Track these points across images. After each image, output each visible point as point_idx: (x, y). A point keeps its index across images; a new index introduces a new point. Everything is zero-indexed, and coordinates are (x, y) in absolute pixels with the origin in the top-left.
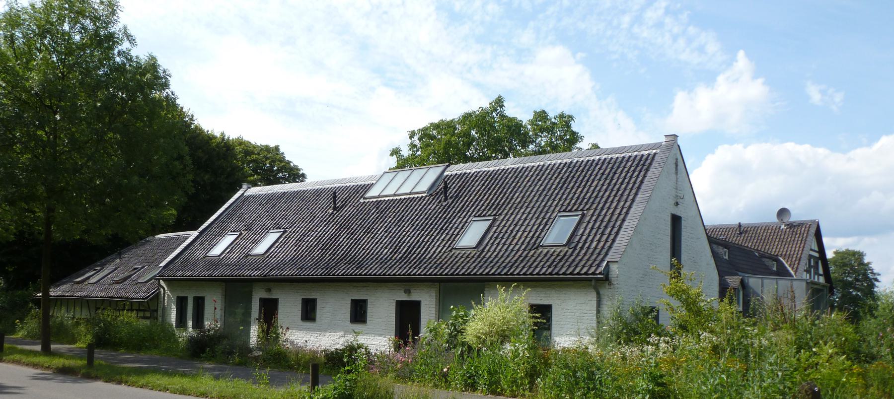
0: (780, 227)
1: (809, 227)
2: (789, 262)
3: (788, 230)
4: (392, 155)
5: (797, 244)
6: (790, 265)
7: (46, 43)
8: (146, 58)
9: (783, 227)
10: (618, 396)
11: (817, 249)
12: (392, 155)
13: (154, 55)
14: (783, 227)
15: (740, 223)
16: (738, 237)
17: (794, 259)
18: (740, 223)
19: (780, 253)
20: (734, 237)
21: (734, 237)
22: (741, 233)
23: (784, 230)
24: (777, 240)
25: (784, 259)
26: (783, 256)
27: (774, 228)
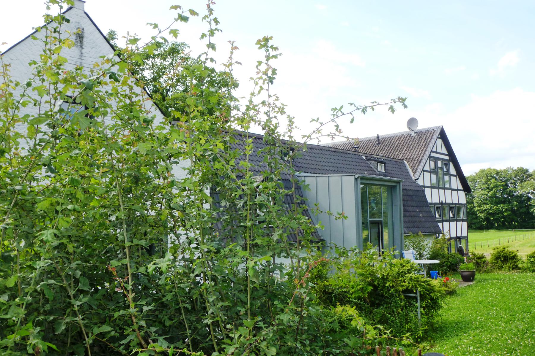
0: (411, 134)
1: (434, 133)
2: (411, 165)
3: (416, 137)
4: (258, 62)
5: (421, 148)
6: (411, 167)
7: (376, 284)
8: (358, 279)
9: (413, 135)
10: (371, 280)
11: (446, 153)
12: (258, 62)
13: (189, 19)
14: (413, 135)
15: (378, 137)
16: (376, 146)
17: (416, 162)
18: (378, 137)
19: (406, 157)
20: (373, 147)
21: (373, 147)
22: (379, 143)
23: (413, 137)
24: (406, 146)
25: (408, 162)
26: (407, 160)
27: (406, 136)
